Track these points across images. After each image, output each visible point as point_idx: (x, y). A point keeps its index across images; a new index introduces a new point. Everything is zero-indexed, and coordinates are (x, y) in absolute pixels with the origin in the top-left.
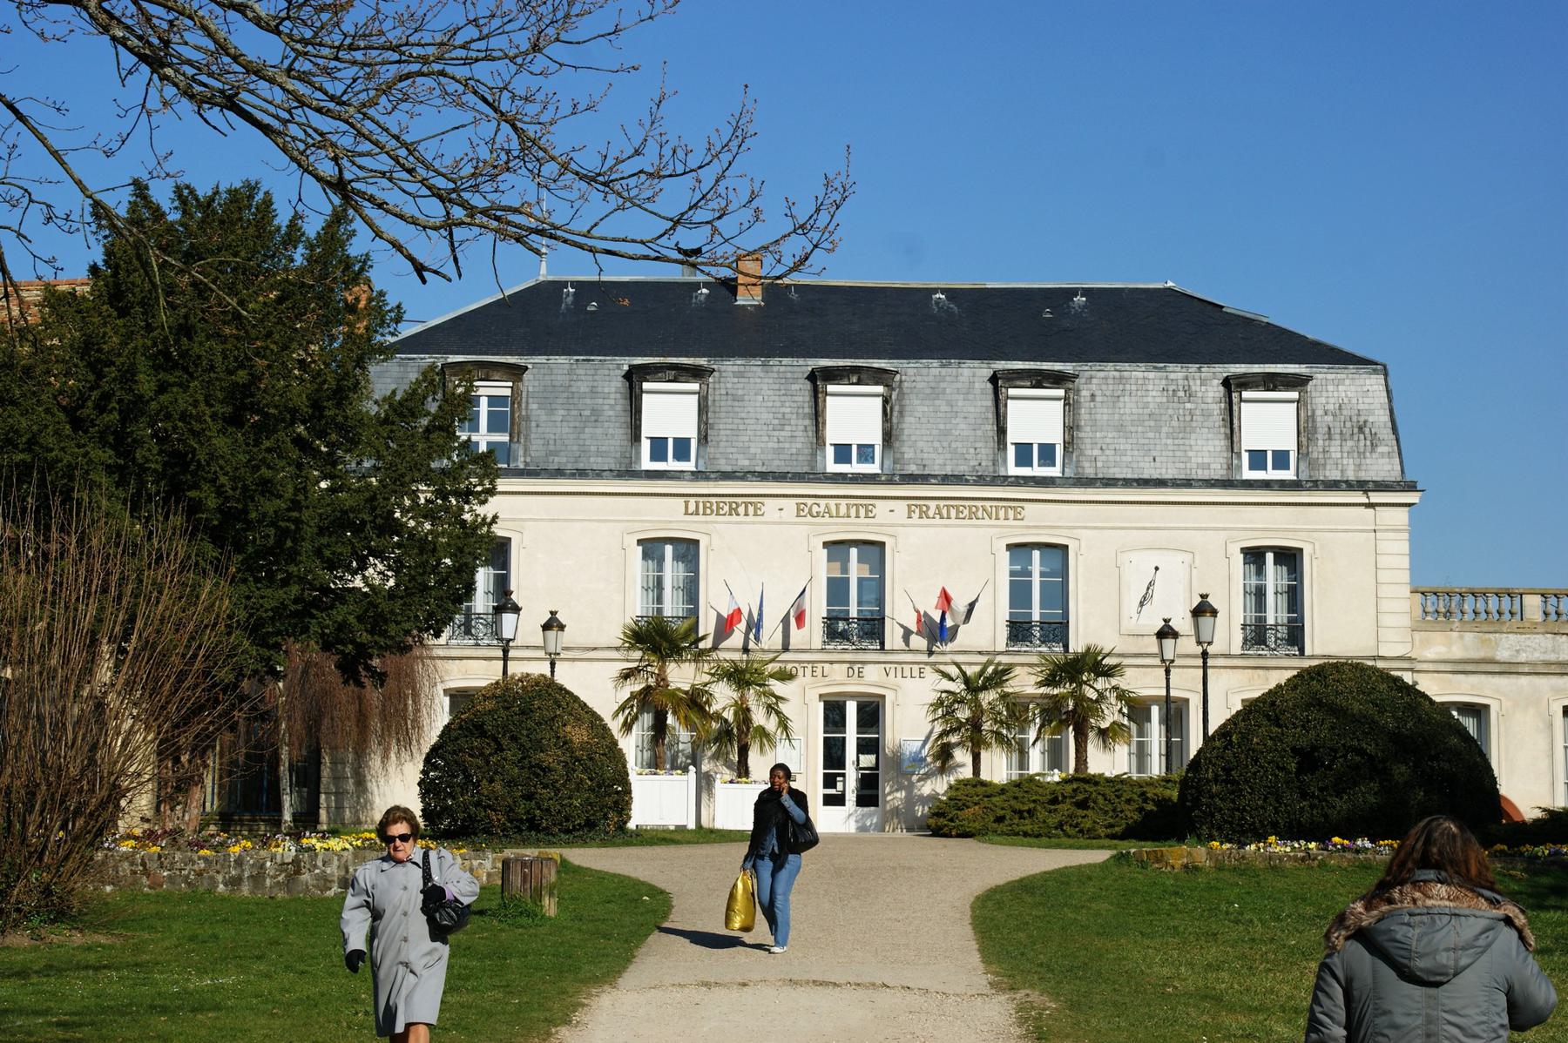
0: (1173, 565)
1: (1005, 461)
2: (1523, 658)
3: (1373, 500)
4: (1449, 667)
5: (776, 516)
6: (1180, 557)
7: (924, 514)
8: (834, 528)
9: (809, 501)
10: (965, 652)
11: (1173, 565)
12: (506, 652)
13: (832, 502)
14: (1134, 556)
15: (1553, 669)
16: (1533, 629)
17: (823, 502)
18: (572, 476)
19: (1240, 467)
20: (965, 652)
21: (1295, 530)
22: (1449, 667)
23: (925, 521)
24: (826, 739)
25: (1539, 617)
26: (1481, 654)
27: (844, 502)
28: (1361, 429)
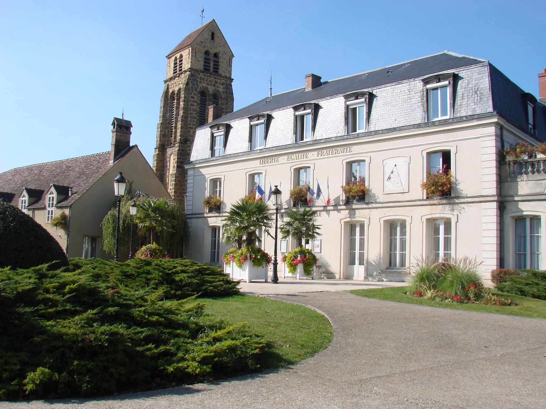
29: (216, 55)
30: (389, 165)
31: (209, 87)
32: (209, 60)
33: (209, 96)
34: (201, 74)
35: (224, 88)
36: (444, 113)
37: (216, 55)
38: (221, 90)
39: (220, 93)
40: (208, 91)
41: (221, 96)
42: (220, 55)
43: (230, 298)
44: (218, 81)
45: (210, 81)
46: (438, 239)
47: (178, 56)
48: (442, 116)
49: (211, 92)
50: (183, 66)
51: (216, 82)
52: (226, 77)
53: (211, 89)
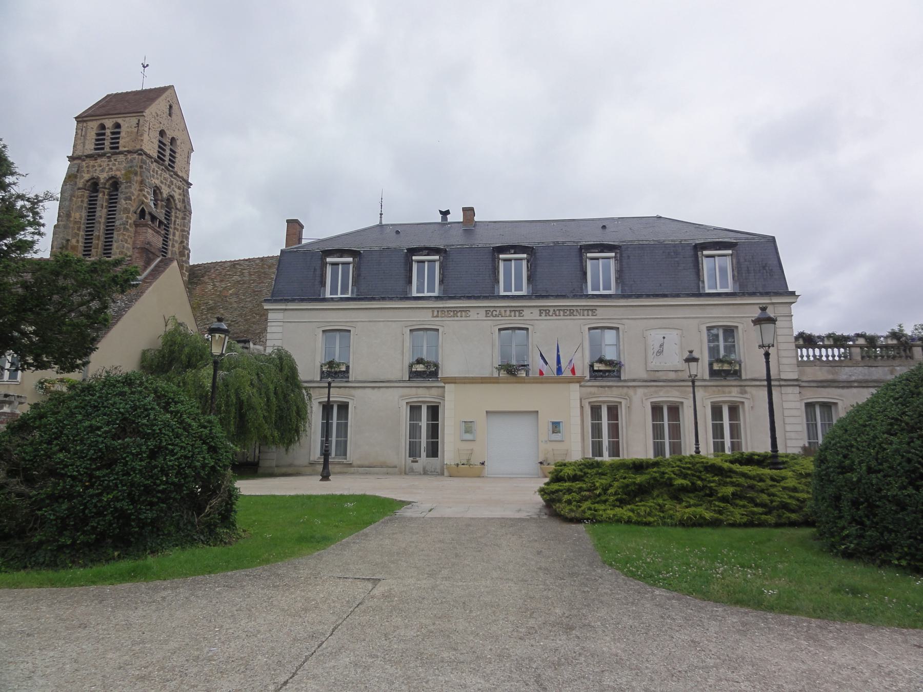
0: (673, 336)
1: (586, 287)
2: (853, 378)
3: (774, 301)
4: (815, 384)
5: (475, 317)
6: (675, 332)
7: (547, 314)
8: (437, 323)
9: (492, 309)
10: (634, 380)
11: (673, 336)
12: (693, 382)
13: (503, 310)
14: (653, 332)
15: (812, 384)
16: (856, 365)
17: (498, 310)
18: (379, 300)
19: (704, 287)
20: (634, 380)
21: (733, 317)
22: (815, 384)
23: (548, 318)
24: (653, 425)
25: (859, 358)
26: (830, 377)
27: (508, 309)
28: (764, 268)
29: (173, 140)
30: (655, 337)
31: (163, 186)
32: (165, 145)
33: (162, 201)
34: (155, 164)
35: (180, 195)
36: (431, 289)
37: (173, 140)
38: (177, 197)
39: (174, 201)
40: (161, 193)
41: (176, 205)
42: (178, 142)
43: (143, 586)
44: (175, 181)
45: (165, 179)
46: (732, 437)
47: (109, 123)
48: (604, 289)
49: (165, 196)
50: (121, 142)
51: (172, 182)
52: (182, 178)
53: (165, 191)
